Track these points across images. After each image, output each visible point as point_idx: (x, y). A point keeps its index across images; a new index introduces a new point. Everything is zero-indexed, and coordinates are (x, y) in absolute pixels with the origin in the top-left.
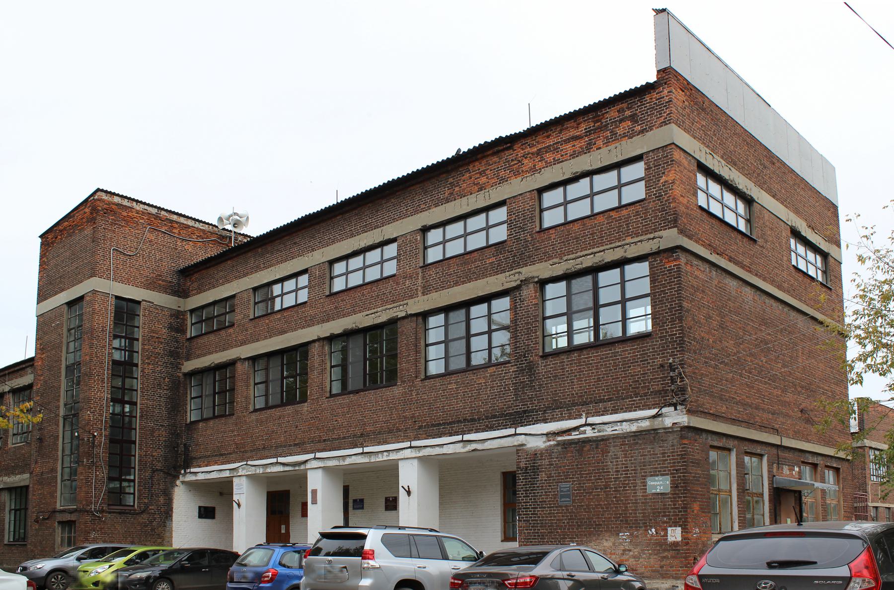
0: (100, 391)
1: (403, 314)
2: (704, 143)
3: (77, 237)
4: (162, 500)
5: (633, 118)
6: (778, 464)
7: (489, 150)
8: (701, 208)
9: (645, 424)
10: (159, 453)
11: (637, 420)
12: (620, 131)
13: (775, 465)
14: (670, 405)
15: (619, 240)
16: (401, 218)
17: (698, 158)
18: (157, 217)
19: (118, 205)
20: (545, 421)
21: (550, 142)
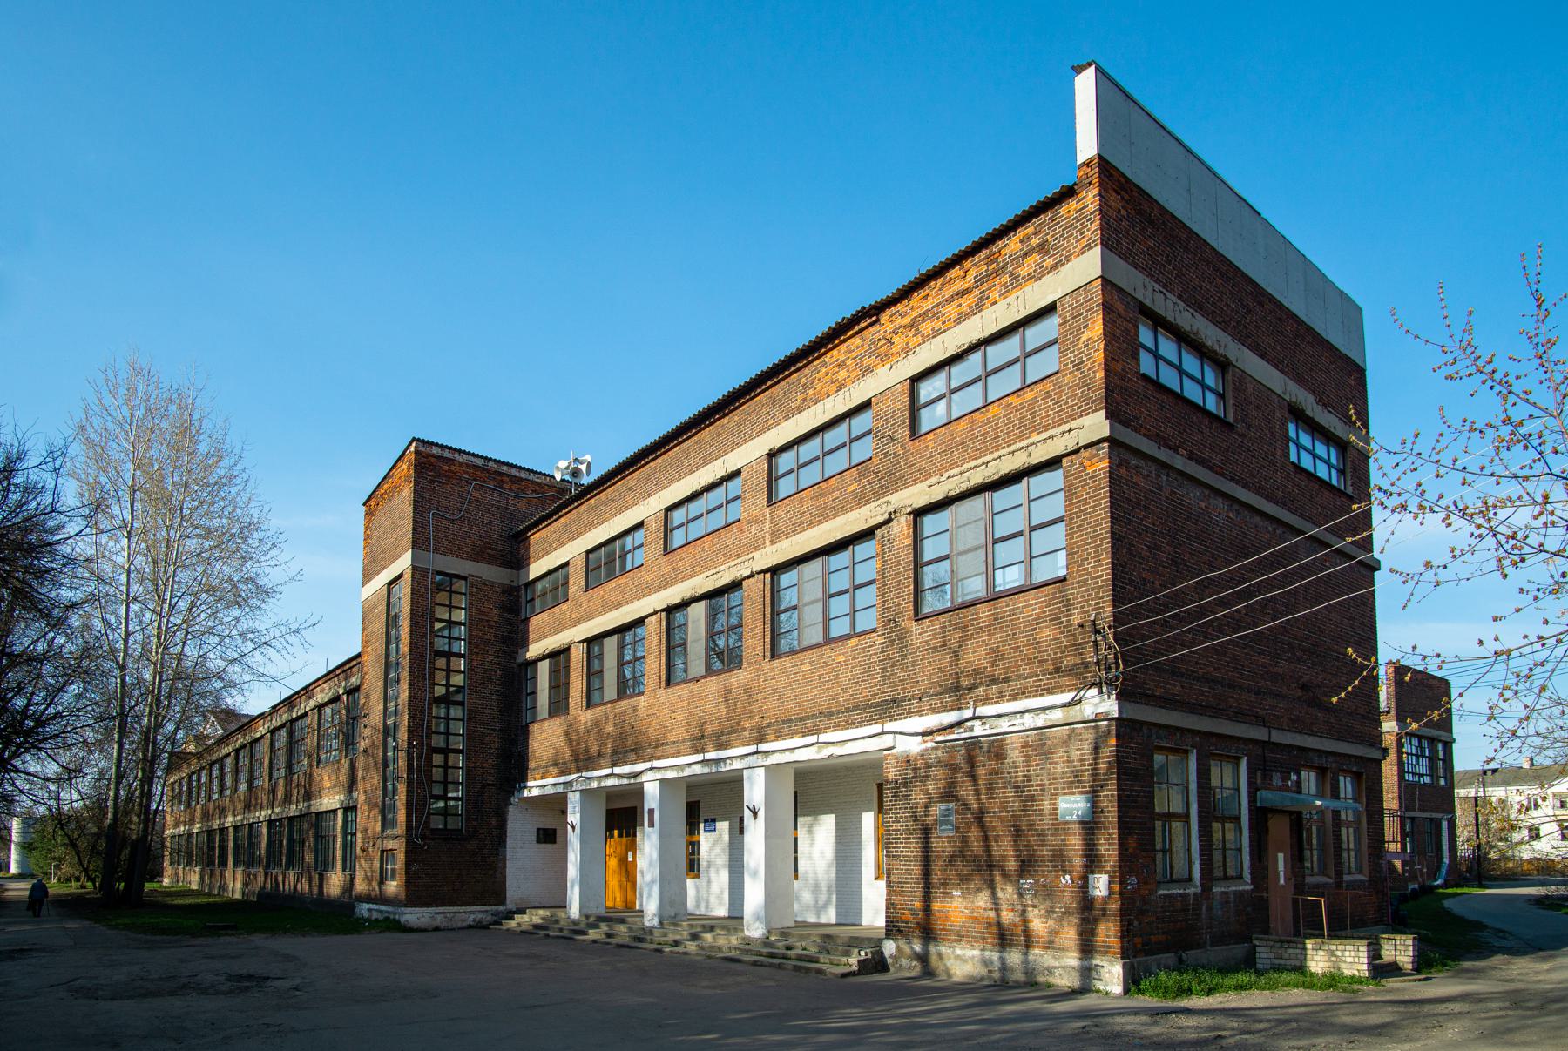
1: (748, 573)
2: (1150, 275)
3: (395, 502)
4: (494, 821)
5: (1042, 248)
6: (1264, 770)
7: (852, 327)
8: (1145, 377)
9: (1057, 716)
10: (491, 763)
11: (1044, 709)
12: (1023, 272)
13: (1259, 773)
14: (1093, 685)
15: (1021, 438)
16: (746, 441)
17: (1141, 298)
18: (483, 469)
19: (439, 457)
21: (928, 305)
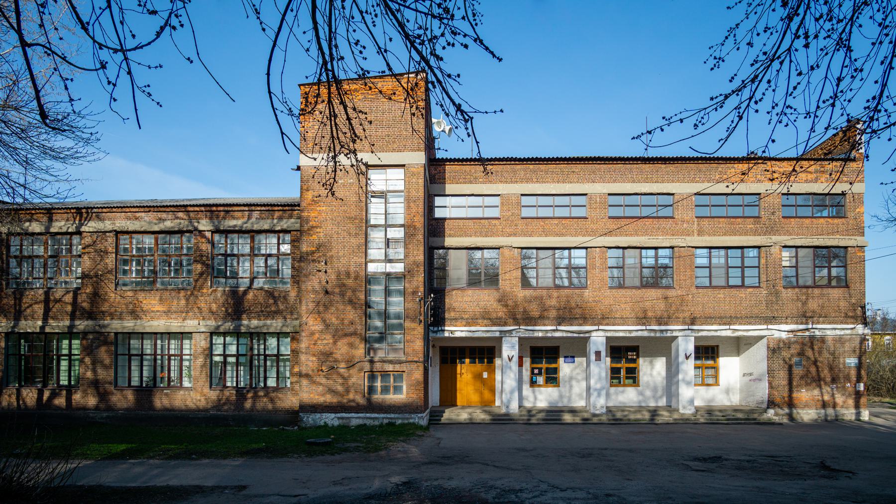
0: (229, 242)
20: (786, 323)
